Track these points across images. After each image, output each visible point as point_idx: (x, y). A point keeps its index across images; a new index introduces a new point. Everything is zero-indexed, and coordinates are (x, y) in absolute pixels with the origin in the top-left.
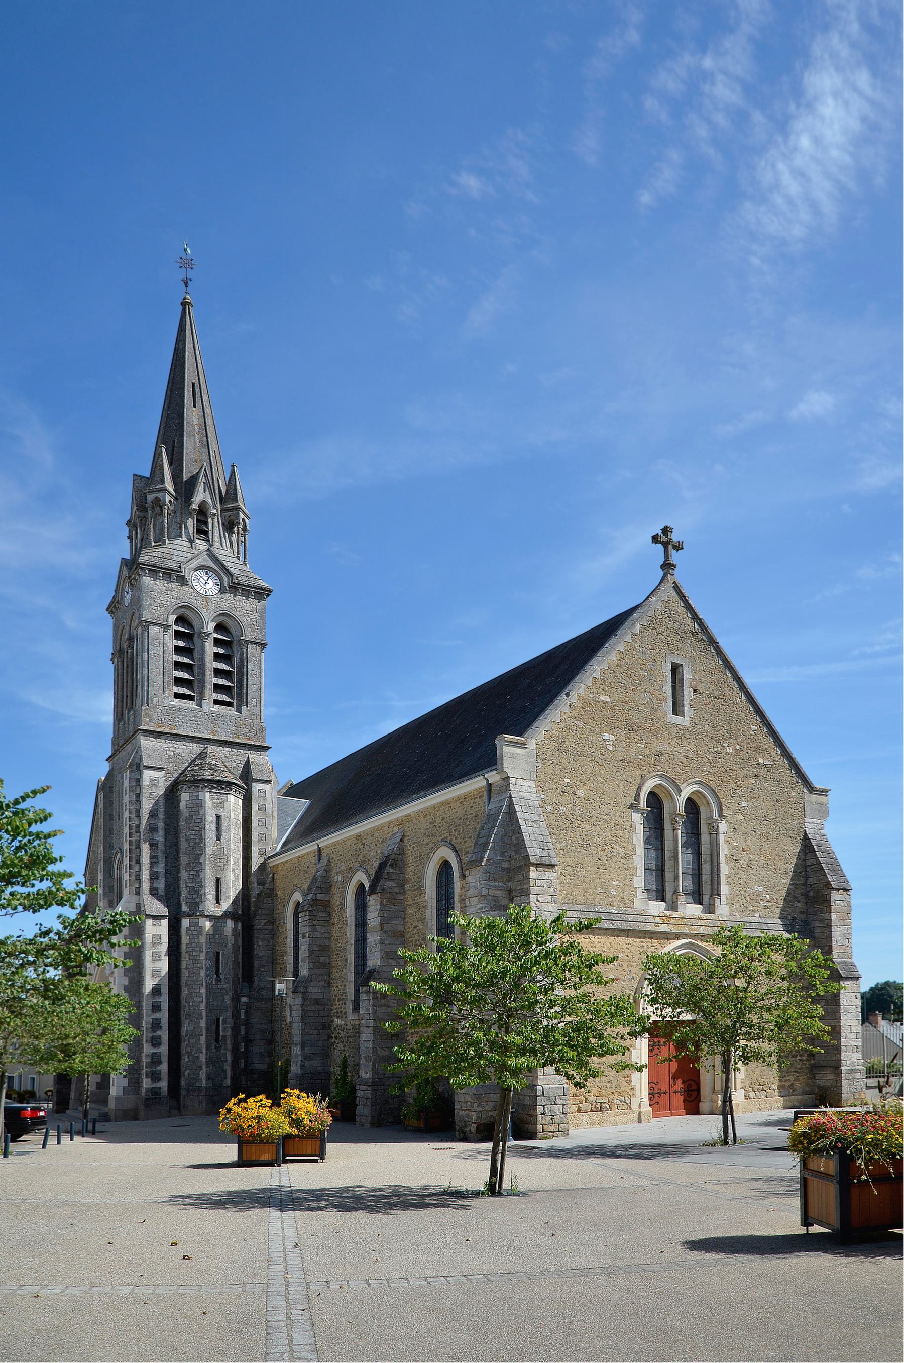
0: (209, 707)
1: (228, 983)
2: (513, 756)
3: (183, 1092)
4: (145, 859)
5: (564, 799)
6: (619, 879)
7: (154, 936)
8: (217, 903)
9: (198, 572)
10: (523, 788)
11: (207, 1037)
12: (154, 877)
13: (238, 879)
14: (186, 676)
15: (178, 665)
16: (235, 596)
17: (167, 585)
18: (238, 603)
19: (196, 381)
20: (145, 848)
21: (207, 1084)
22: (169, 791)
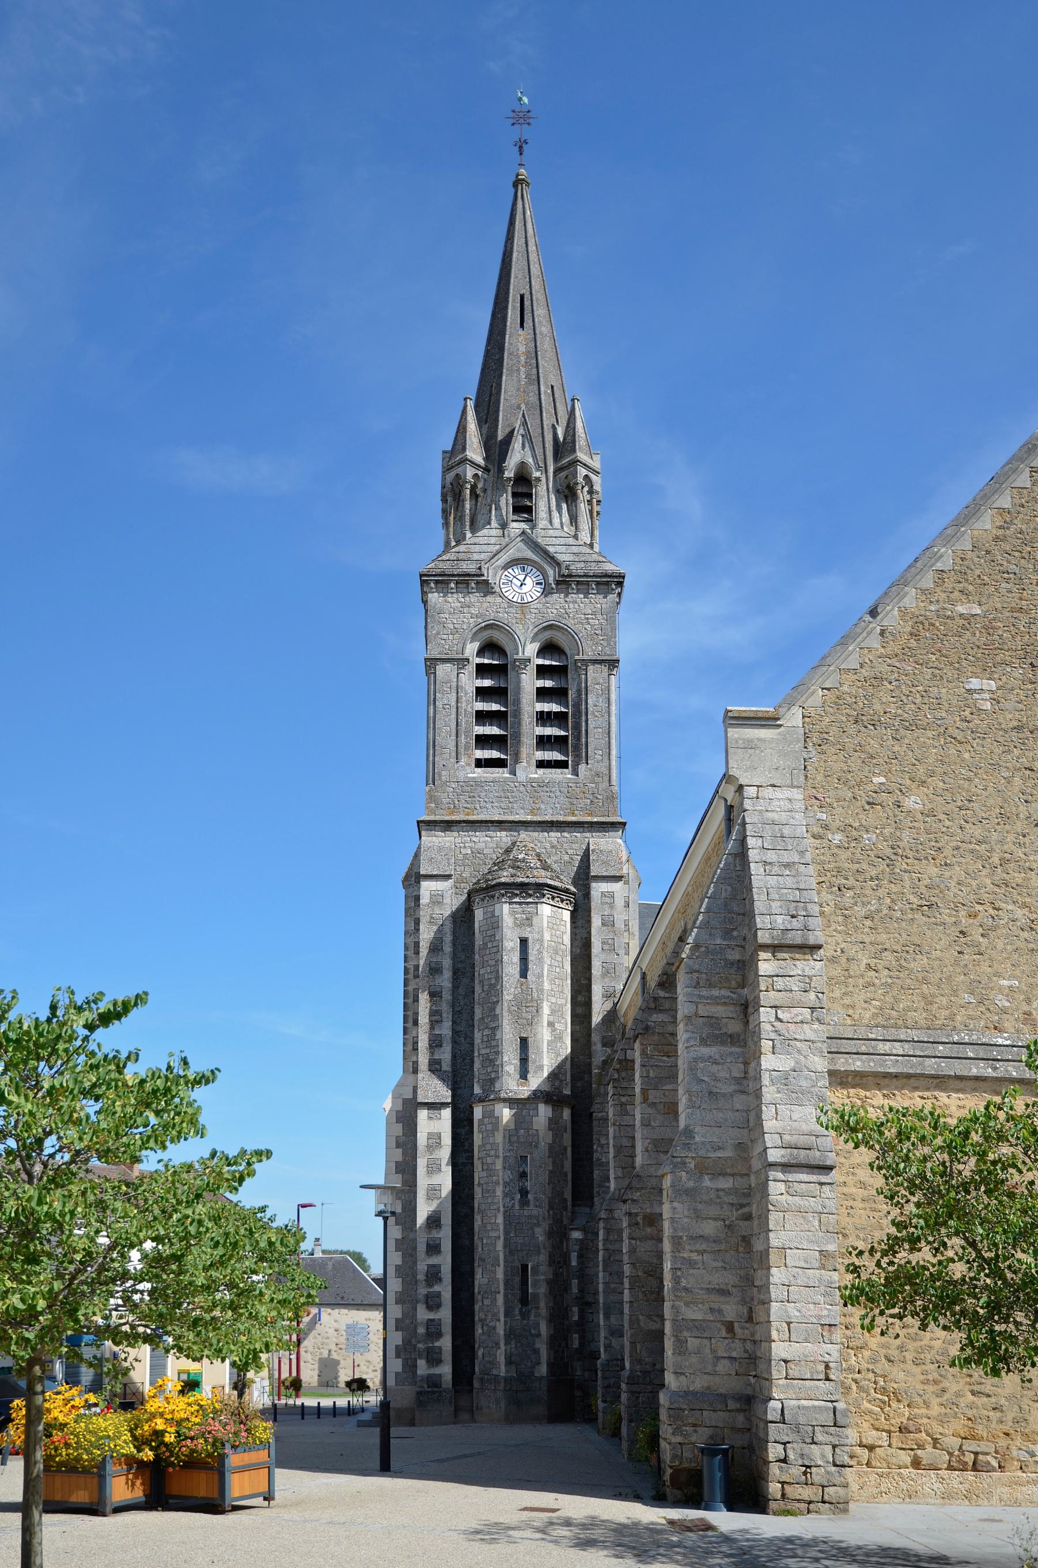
0: (527, 771)
1: (540, 1207)
2: (750, 745)
3: (476, 1384)
4: (424, 1018)
5: (872, 817)
6: (1018, 972)
7: (430, 1136)
8: (521, 1077)
9: (510, 570)
10: (775, 803)
11: (506, 1295)
12: (435, 1043)
13: (561, 1038)
14: (495, 730)
15: (482, 717)
16: (566, 596)
17: (463, 600)
18: (571, 606)
19: (525, 291)
20: (424, 998)
21: (507, 1371)
22: (464, 910)
